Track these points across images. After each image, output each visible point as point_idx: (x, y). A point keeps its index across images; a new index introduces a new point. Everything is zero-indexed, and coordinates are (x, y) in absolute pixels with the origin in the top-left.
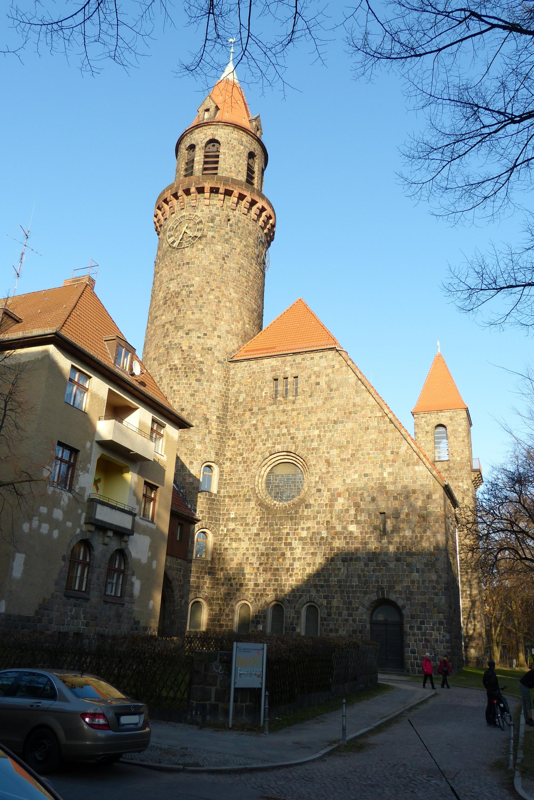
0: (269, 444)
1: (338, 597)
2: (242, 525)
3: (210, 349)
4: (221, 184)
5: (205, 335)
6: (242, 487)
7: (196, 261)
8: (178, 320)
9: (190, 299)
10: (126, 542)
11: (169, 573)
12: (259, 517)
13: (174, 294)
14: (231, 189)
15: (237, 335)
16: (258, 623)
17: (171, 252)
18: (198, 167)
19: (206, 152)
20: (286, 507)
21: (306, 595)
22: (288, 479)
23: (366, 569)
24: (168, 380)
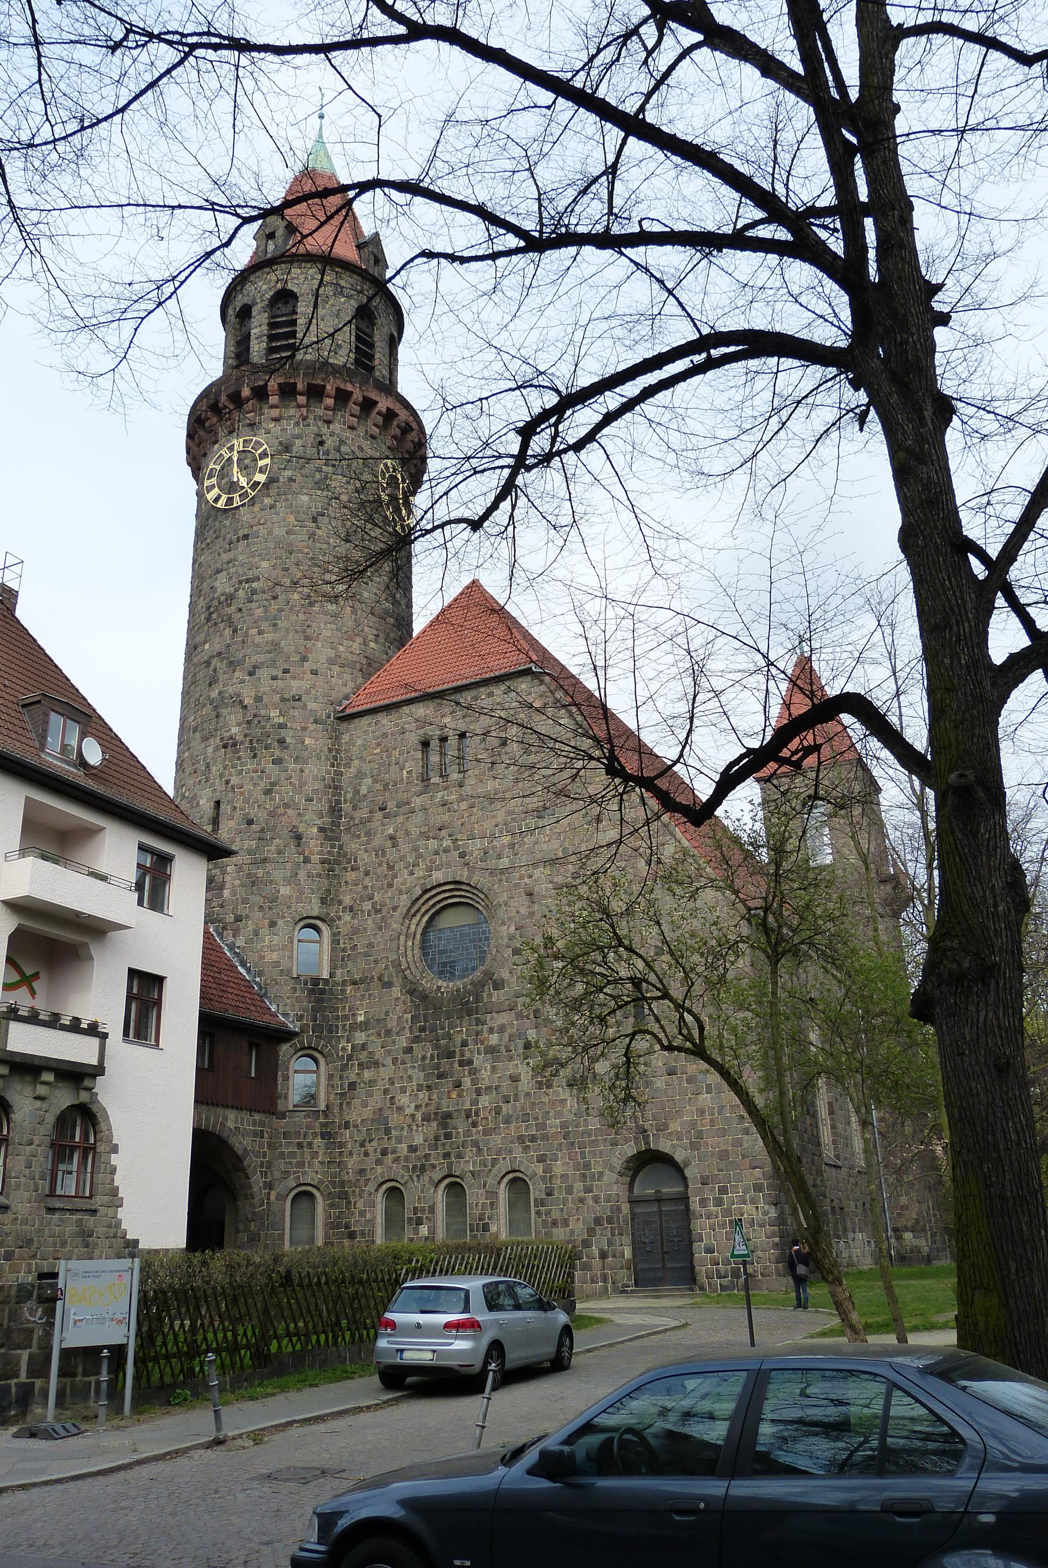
0: (420, 872)
1: (563, 1155)
2: (379, 1034)
6: (376, 962)
7: (262, 531)
9: (254, 605)
10: (90, 1089)
13: (222, 598)
15: (352, 665)
16: (419, 1222)
17: (216, 518)
19: (273, 317)
22: (461, 936)
24: (220, 767)
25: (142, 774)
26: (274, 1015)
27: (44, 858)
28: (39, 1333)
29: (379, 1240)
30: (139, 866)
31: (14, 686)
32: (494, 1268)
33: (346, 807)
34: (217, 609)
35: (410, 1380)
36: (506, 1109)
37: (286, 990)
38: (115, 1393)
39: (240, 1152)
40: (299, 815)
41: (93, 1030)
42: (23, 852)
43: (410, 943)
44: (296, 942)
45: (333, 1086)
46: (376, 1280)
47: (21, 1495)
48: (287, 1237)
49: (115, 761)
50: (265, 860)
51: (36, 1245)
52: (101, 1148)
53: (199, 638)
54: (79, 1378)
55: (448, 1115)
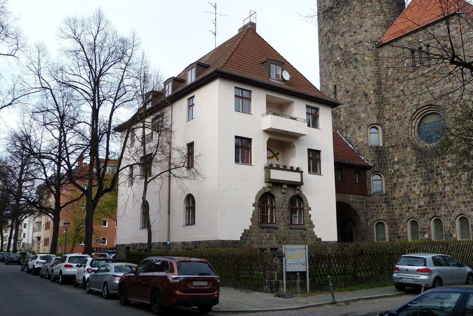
5: (355, 32)
6: (400, 138)
12: (415, 158)
15: (380, 25)
16: (424, 233)
20: (434, 147)
21: (457, 210)
24: (335, 73)
25: (305, 80)
26: (363, 161)
27: (274, 114)
28: (279, 267)
29: (410, 239)
30: (307, 113)
31: (258, 57)
32: (438, 250)
33: (383, 81)
35: (407, 288)
36: (456, 191)
37: (367, 151)
38: (303, 285)
39: (355, 209)
40: (365, 86)
41: (298, 170)
42: (268, 113)
43: (413, 130)
44: (369, 134)
45: (387, 185)
46: (396, 254)
47: (271, 313)
48: (375, 238)
49: (294, 77)
50: (354, 105)
51: (288, 239)
52: (305, 209)
53: (322, 26)
54: (293, 281)
55: (433, 194)
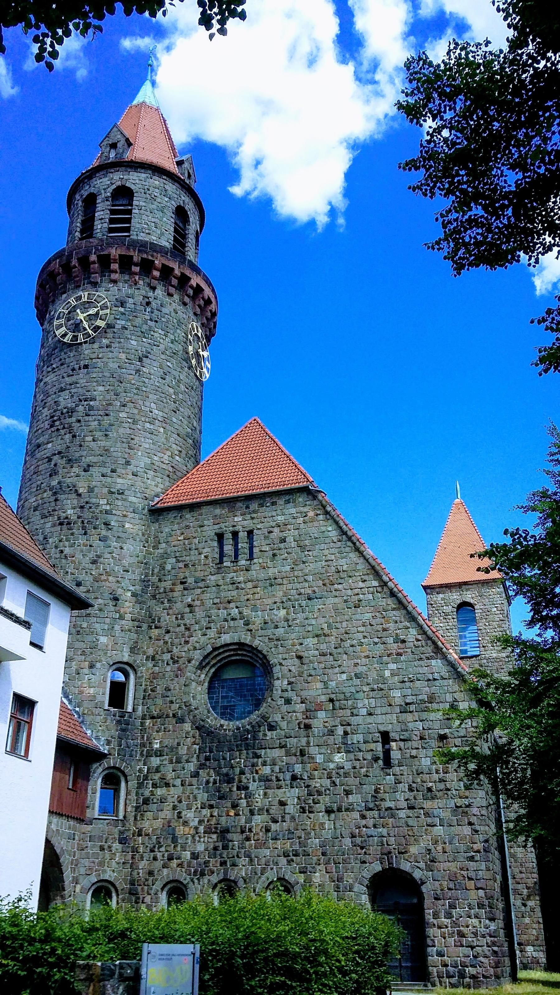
0: (212, 633)
3: (121, 493)
4: (134, 251)
8: (72, 450)
11: (54, 841)
13: (65, 411)
14: (150, 258)
18: (100, 226)
20: (238, 729)
21: (272, 869)
22: (241, 686)
23: (364, 822)
34: (59, 419)
